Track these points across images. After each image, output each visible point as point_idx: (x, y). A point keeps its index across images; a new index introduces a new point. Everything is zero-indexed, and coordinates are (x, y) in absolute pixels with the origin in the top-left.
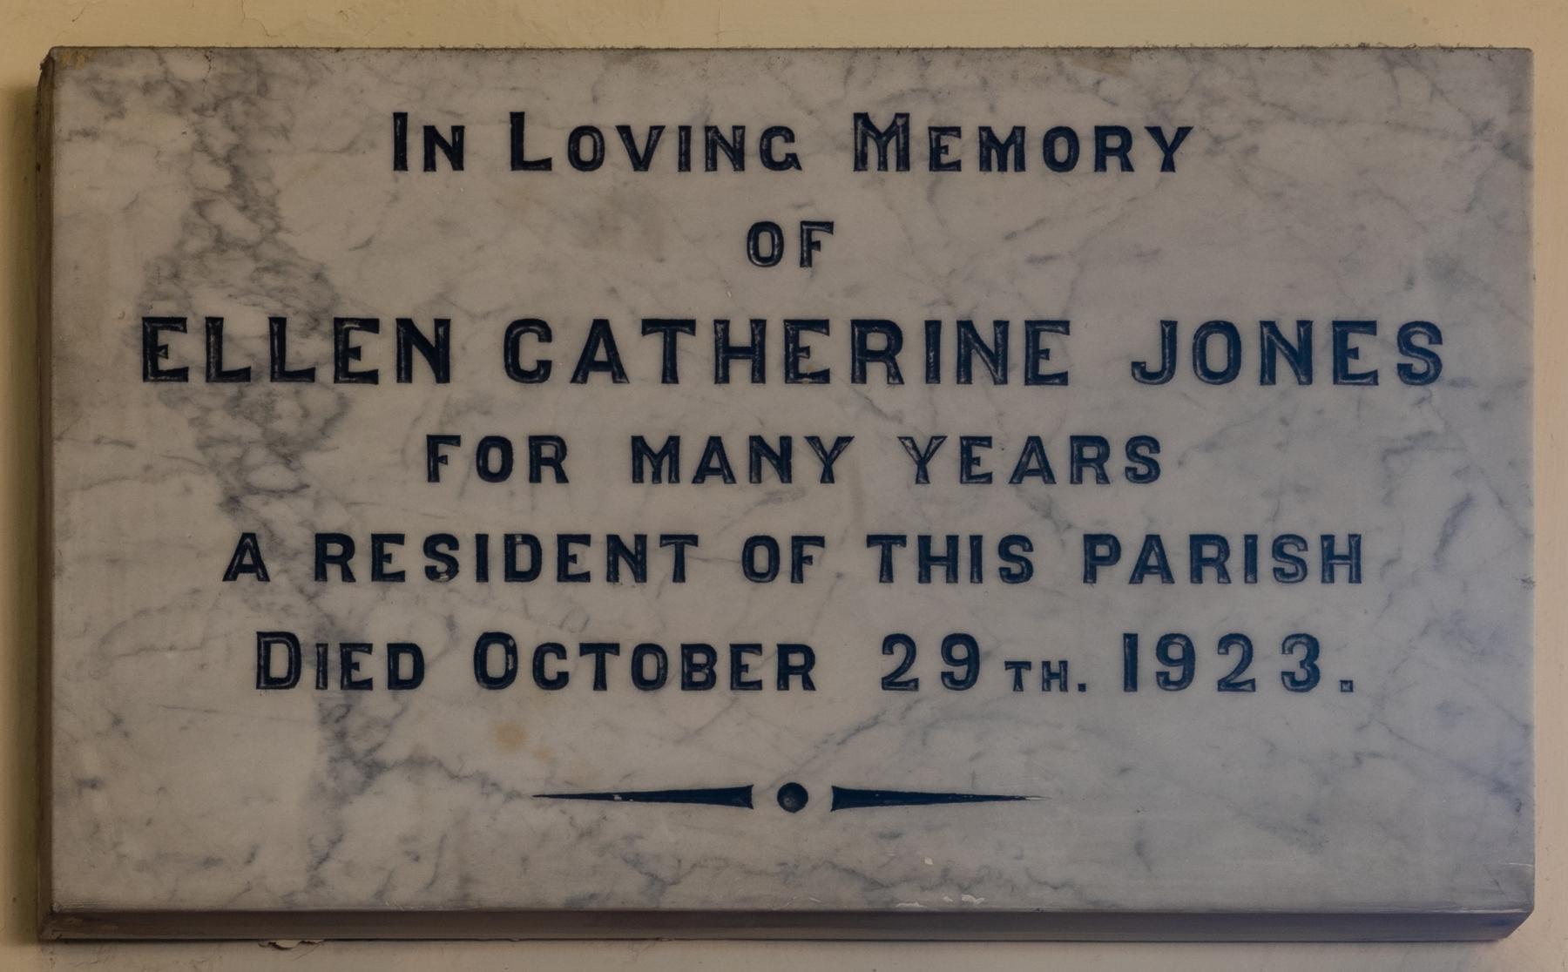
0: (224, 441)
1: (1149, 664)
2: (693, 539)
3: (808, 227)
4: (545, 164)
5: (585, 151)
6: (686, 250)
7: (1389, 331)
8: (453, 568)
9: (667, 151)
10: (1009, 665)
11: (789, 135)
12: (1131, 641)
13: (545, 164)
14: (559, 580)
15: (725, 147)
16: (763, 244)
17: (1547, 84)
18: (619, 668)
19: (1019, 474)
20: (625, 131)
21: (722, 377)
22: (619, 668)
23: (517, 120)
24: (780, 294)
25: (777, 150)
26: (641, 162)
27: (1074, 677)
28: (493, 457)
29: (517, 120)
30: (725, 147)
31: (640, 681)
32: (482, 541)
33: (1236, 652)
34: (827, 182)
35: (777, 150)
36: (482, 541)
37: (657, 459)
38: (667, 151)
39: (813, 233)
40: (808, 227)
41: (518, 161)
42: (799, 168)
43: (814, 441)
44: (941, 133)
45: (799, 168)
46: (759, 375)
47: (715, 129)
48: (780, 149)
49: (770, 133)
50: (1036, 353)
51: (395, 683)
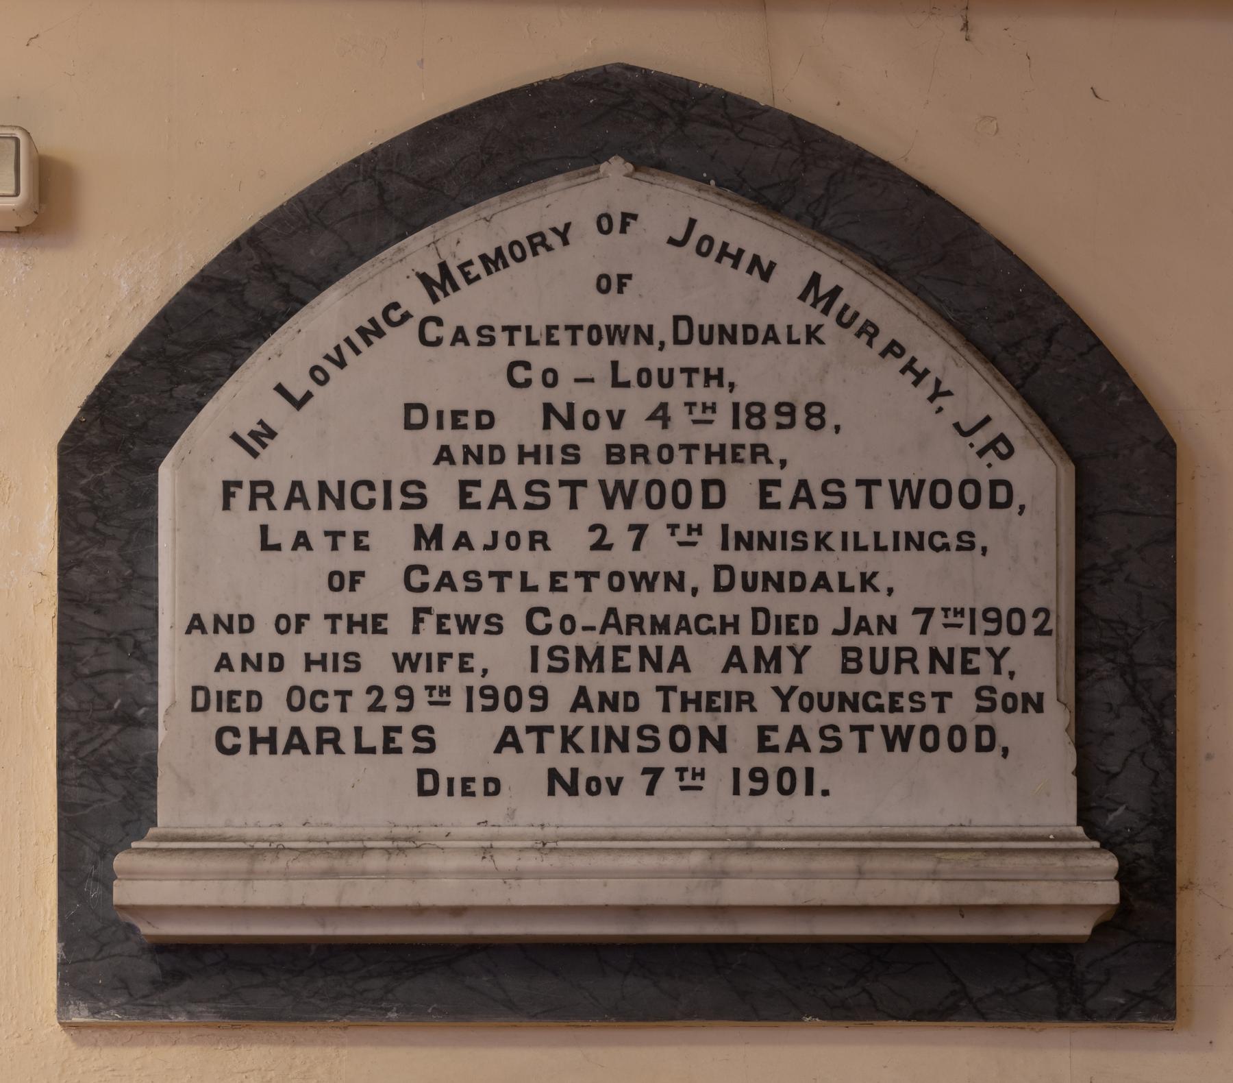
0: (926, 277)
4: (308, 396)
5: (318, 375)
9: (347, 351)
13: (308, 396)
18: (582, 336)
19: (495, 500)
20: (327, 357)
21: (736, 617)
22: (582, 336)
23: (280, 389)
26: (341, 364)
27: (831, 421)
29: (280, 389)
31: (591, 342)
37: (495, 263)
38: (347, 351)
41: (298, 404)
46: (725, 245)
47: (380, 337)
48: (395, 315)
50: (965, 662)
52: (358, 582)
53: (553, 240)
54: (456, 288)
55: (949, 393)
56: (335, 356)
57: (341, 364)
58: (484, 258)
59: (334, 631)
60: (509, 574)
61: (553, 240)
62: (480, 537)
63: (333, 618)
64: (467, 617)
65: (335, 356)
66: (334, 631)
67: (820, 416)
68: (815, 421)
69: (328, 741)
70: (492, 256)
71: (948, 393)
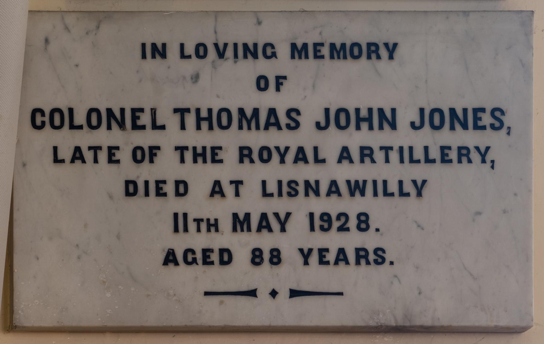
1: (317, 223)
2: (241, 182)
3: (278, 78)
6: (231, 86)
7: (488, 111)
8: (297, 193)
10: (195, 220)
11: (273, 46)
12: (311, 215)
14: (176, 196)
15: (250, 51)
16: (262, 84)
17: (538, 23)
20: (216, 45)
23: (55, 149)
24: (268, 100)
25: (269, 51)
28: (199, 155)
30: (250, 51)
32: (147, 183)
33: (343, 219)
34: (283, 64)
35: (269, 51)
36: (375, 182)
38: (230, 52)
39: (280, 80)
40: (278, 78)
42: (276, 58)
43: (477, 148)
44: (317, 46)
45: (276, 58)
49: (266, 45)
51: (178, 194)
52: (282, 84)
53: (383, 52)
54: (307, 57)
55: (488, 148)
56: (221, 47)
57: (221, 55)
58: (333, 46)
59: (182, 161)
60: (391, 148)
61: (383, 52)
62: (330, 152)
63: (181, 149)
64: (357, 182)
65: (221, 47)
66: (182, 161)
67: (366, 222)
68: (363, 226)
69: (367, 155)
70: (338, 47)
71: (488, 148)
